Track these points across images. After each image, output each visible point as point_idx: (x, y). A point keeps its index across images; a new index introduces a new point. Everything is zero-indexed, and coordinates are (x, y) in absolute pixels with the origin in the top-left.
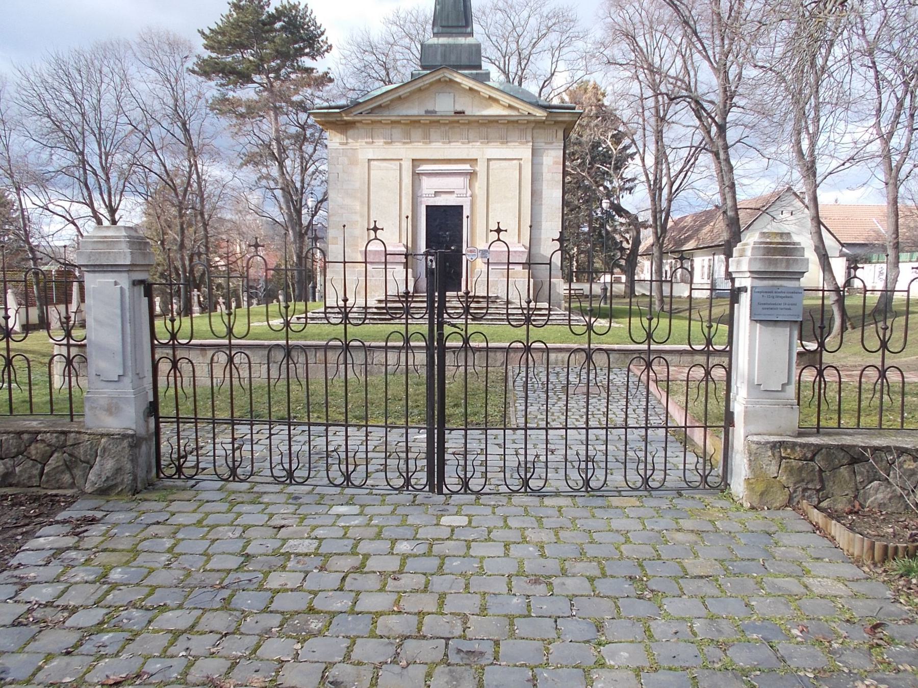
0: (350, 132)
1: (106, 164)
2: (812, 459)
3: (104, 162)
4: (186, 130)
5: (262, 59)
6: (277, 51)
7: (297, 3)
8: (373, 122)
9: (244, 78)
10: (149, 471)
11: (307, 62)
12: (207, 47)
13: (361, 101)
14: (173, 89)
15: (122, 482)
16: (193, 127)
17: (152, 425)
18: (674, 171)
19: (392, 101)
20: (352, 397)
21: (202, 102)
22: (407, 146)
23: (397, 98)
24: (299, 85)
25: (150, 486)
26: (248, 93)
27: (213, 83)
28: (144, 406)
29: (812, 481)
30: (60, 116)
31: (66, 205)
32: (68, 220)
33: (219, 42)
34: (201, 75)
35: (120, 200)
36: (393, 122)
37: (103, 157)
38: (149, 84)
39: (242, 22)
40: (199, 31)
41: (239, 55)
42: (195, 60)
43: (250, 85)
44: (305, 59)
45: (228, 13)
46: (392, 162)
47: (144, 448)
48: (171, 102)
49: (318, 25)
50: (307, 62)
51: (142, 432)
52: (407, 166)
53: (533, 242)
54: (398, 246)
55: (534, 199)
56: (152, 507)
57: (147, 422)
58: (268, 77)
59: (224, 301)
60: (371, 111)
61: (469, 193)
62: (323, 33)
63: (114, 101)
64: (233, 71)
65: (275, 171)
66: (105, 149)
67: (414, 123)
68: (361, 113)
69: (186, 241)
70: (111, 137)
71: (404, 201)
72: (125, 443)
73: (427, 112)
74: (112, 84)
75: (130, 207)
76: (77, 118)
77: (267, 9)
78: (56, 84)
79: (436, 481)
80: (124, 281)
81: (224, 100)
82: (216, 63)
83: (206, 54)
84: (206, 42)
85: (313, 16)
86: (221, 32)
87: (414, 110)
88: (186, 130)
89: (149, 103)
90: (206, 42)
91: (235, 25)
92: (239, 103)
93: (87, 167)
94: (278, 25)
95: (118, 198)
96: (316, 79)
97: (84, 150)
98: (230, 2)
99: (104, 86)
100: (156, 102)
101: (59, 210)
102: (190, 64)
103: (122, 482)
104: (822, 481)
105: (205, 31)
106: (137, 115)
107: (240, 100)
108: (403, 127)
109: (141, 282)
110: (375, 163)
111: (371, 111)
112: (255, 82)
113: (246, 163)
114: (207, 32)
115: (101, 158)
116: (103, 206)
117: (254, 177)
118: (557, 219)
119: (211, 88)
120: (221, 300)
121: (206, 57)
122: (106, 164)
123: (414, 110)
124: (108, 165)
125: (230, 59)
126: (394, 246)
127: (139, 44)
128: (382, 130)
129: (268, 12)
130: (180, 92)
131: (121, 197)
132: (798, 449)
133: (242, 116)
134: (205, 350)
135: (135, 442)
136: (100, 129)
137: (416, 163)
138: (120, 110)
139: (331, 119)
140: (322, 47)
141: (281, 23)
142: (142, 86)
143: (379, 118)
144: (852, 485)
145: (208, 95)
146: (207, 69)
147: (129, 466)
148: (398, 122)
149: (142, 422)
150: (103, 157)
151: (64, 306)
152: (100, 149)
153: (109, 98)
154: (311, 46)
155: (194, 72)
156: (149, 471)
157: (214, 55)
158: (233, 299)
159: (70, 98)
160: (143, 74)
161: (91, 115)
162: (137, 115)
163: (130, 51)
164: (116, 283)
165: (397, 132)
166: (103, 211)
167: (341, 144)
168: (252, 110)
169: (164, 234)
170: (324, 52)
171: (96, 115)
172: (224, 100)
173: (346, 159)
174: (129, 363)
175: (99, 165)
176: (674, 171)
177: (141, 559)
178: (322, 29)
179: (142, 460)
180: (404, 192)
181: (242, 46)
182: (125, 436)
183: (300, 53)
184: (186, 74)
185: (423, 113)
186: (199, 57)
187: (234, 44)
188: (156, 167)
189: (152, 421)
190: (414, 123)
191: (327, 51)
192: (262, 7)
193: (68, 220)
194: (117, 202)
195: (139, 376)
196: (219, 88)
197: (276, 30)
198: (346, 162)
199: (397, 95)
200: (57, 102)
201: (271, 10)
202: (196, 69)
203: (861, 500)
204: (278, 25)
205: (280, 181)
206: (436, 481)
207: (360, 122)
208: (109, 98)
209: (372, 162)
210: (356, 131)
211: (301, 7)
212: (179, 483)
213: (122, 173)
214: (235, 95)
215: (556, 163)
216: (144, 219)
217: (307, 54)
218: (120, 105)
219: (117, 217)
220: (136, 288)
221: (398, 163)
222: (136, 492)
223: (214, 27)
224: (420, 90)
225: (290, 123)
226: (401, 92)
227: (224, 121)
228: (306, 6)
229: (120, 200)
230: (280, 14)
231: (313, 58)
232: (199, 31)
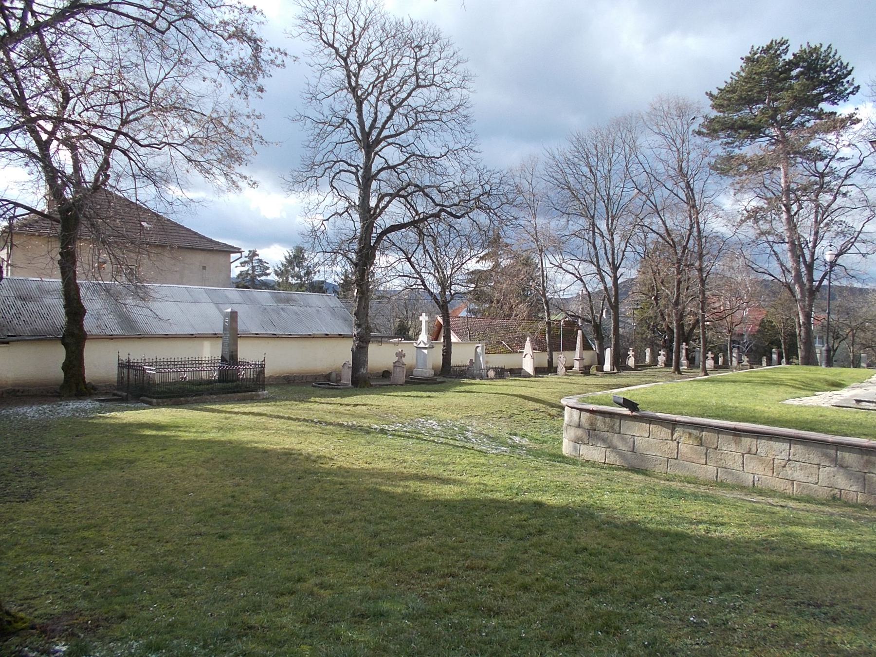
1: (612, 226)
3: (610, 223)
5: (776, 110)
6: (795, 98)
7: (818, 46)
9: (754, 130)
11: (826, 107)
12: (713, 107)
21: (707, 160)
26: (752, 149)
27: (720, 142)
30: (578, 186)
31: (577, 264)
32: (577, 277)
33: (729, 99)
34: (708, 135)
35: (622, 259)
39: (755, 74)
40: (707, 93)
42: (701, 120)
49: (845, 64)
50: (826, 107)
58: (779, 129)
59: (713, 356)
62: (849, 73)
64: (744, 126)
65: (781, 227)
70: (617, 203)
76: (590, 187)
78: (576, 160)
81: (730, 158)
83: (714, 114)
85: (837, 57)
91: (748, 79)
93: (596, 230)
97: (594, 215)
98: (744, 57)
101: (570, 268)
102: (695, 127)
105: (713, 93)
106: (642, 179)
115: (608, 220)
119: (717, 148)
120: (710, 355)
122: (612, 226)
127: (649, 114)
134: (740, 436)
140: (846, 89)
145: (714, 153)
146: (712, 129)
153: (618, 168)
154: (831, 89)
155: (699, 133)
158: (721, 354)
159: (586, 170)
161: (601, 183)
162: (642, 179)
166: (607, 268)
170: (848, 94)
175: (606, 228)
178: (849, 68)
181: (750, 101)
183: (819, 98)
187: (745, 98)
191: (852, 93)
193: (577, 277)
197: (792, 78)
200: (576, 175)
201: (789, 57)
202: (705, 131)
204: (794, 73)
217: (826, 99)
223: (723, 86)
225: (801, 173)
229: (622, 259)
231: (834, 103)
232: (707, 93)
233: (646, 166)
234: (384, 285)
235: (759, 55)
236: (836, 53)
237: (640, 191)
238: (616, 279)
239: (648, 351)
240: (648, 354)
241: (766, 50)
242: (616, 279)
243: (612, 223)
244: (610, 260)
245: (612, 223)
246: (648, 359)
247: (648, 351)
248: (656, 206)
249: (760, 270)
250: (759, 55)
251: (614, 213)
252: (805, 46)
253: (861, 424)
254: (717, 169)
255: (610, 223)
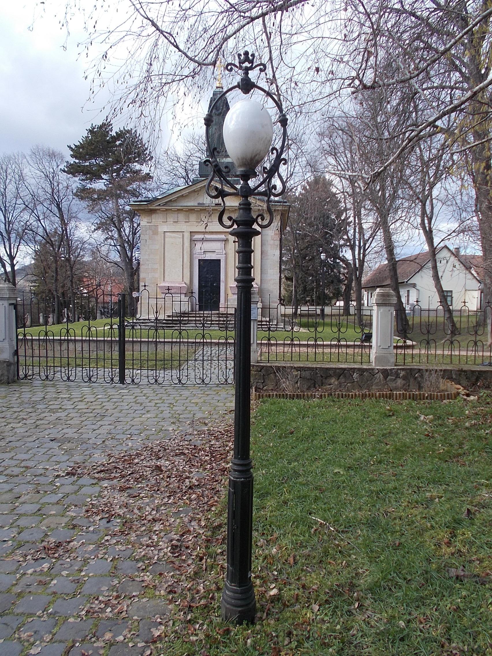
0: (154, 216)
1: (9, 229)
2: (260, 371)
3: (7, 227)
4: (60, 209)
8: (167, 210)
9: (95, 176)
10: (14, 376)
11: (137, 166)
12: (72, 156)
13: (159, 197)
14: (51, 182)
15: (3, 379)
16: (64, 205)
17: (16, 359)
18: (366, 237)
19: (178, 197)
20: (478, 457)
22: (187, 224)
23: (181, 196)
24: (132, 180)
25: (14, 382)
26: (100, 185)
27: (77, 179)
28: (13, 351)
29: (260, 379)
33: (81, 153)
35: (17, 252)
36: (178, 210)
37: (7, 225)
38: (37, 180)
41: (93, 161)
43: (100, 181)
44: (135, 164)
45: (86, 135)
46: (178, 233)
47: (12, 367)
48: (50, 191)
50: (137, 166)
51: (12, 361)
52: (187, 235)
53: (263, 281)
54: (182, 284)
55: (263, 256)
56: (15, 387)
57: (14, 357)
60: (166, 204)
61: (224, 252)
62: (146, 149)
63: (14, 190)
66: (8, 219)
67: (191, 210)
68: (160, 205)
69: (59, 277)
71: (185, 257)
72: (5, 365)
73: (199, 204)
74: (13, 179)
75: (23, 256)
77: (110, 133)
79: (122, 380)
80: (6, 303)
81: (83, 190)
82: (79, 167)
83: (72, 160)
84: (72, 153)
86: (82, 146)
87: (191, 203)
88: (60, 209)
89: (35, 191)
90: (72, 153)
92: (94, 191)
94: (118, 143)
95: (16, 250)
96: (143, 177)
99: (8, 181)
100: (40, 191)
103: (3, 379)
104: (264, 379)
105: (71, 146)
106: (28, 198)
107: (94, 190)
108: (185, 212)
109: (13, 304)
110: (168, 234)
111: (166, 204)
112: (103, 179)
113: (98, 228)
114: (73, 147)
115: (6, 226)
116: (6, 255)
117: (103, 237)
118: (276, 268)
121: (72, 163)
122: (9, 229)
123: (191, 203)
124: (10, 229)
125: (88, 164)
126: (179, 284)
128: (172, 215)
129: (111, 135)
130: (56, 184)
131: (17, 249)
132: (255, 367)
133: (94, 200)
135: (9, 364)
136: (5, 207)
137: (192, 234)
138: (17, 196)
139: (142, 208)
141: (120, 142)
142: (32, 181)
143: (170, 208)
144: (275, 381)
147: (6, 373)
148: (182, 210)
149: (12, 357)
150: (7, 225)
151: (470, 326)
152: (5, 220)
155: (64, 171)
156: (14, 376)
157: (77, 161)
160: (33, 173)
163: (25, 160)
164: (3, 304)
165: (181, 217)
167: (148, 222)
168: (102, 195)
169: (46, 273)
170: (148, 160)
171: (3, 198)
172: (83, 190)
173: (151, 231)
174: (7, 334)
176: (366, 237)
177: (7, 398)
179: (11, 372)
180: (185, 252)
181: (93, 156)
182: (5, 362)
184: (60, 173)
185: (196, 205)
186: (67, 162)
188: (41, 231)
189: (16, 357)
190: (191, 210)
192: (108, 132)
194: (15, 253)
195: (11, 340)
196: (81, 182)
197: (116, 146)
198: (151, 233)
199: (181, 194)
201: (113, 133)
202: (66, 169)
203: (278, 386)
204: (118, 143)
205: (119, 240)
206: (122, 380)
207: (159, 209)
208: (11, 188)
209: (166, 234)
210: (157, 215)
211: (133, 132)
212: (26, 381)
213: (18, 234)
214: (91, 186)
215: (275, 234)
216: (33, 262)
217: (136, 162)
218: (18, 193)
219: (15, 262)
220: (11, 306)
221: (181, 234)
222: (9, 383)
224: (194, 191)
226: (184, 192)
227: (84, 204)
228: (135, 131)
229: (17, 252)
230: (120, 135)
233: (31, 191)
234: (10, 469)
235: (96, 129)
236: (140, 135)
237: (27, 206)
238: (13, 266)
239: (357, 266)
240: (41, 318)
241: (101, 127)
242: (13, 266)
243: (9, 226)
244: (9, 253)
245: (9, 226)
246: (41, 320)
247: (357, 266)
248: (38, 217)
249: (109, 261)
250: (96, 129)
251: (10, 219)
252: (122, 129)
253: (466, 378)
254: (77, 196)
255: (7, 227)
